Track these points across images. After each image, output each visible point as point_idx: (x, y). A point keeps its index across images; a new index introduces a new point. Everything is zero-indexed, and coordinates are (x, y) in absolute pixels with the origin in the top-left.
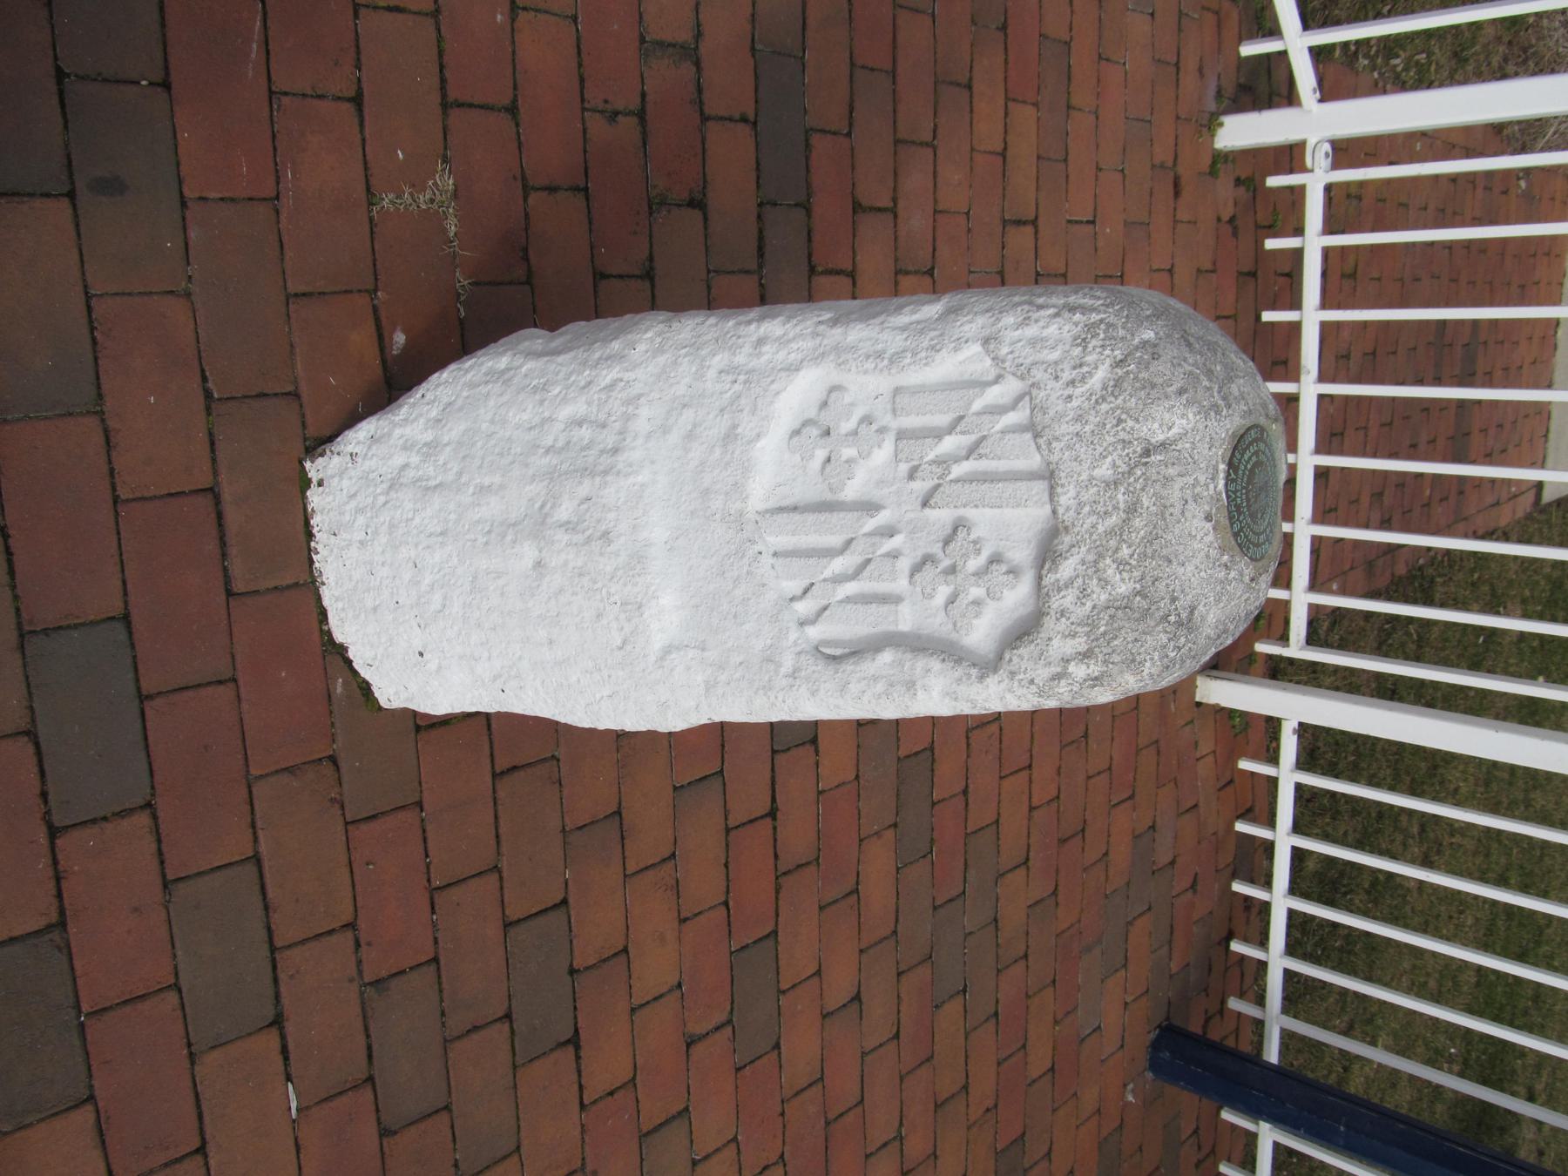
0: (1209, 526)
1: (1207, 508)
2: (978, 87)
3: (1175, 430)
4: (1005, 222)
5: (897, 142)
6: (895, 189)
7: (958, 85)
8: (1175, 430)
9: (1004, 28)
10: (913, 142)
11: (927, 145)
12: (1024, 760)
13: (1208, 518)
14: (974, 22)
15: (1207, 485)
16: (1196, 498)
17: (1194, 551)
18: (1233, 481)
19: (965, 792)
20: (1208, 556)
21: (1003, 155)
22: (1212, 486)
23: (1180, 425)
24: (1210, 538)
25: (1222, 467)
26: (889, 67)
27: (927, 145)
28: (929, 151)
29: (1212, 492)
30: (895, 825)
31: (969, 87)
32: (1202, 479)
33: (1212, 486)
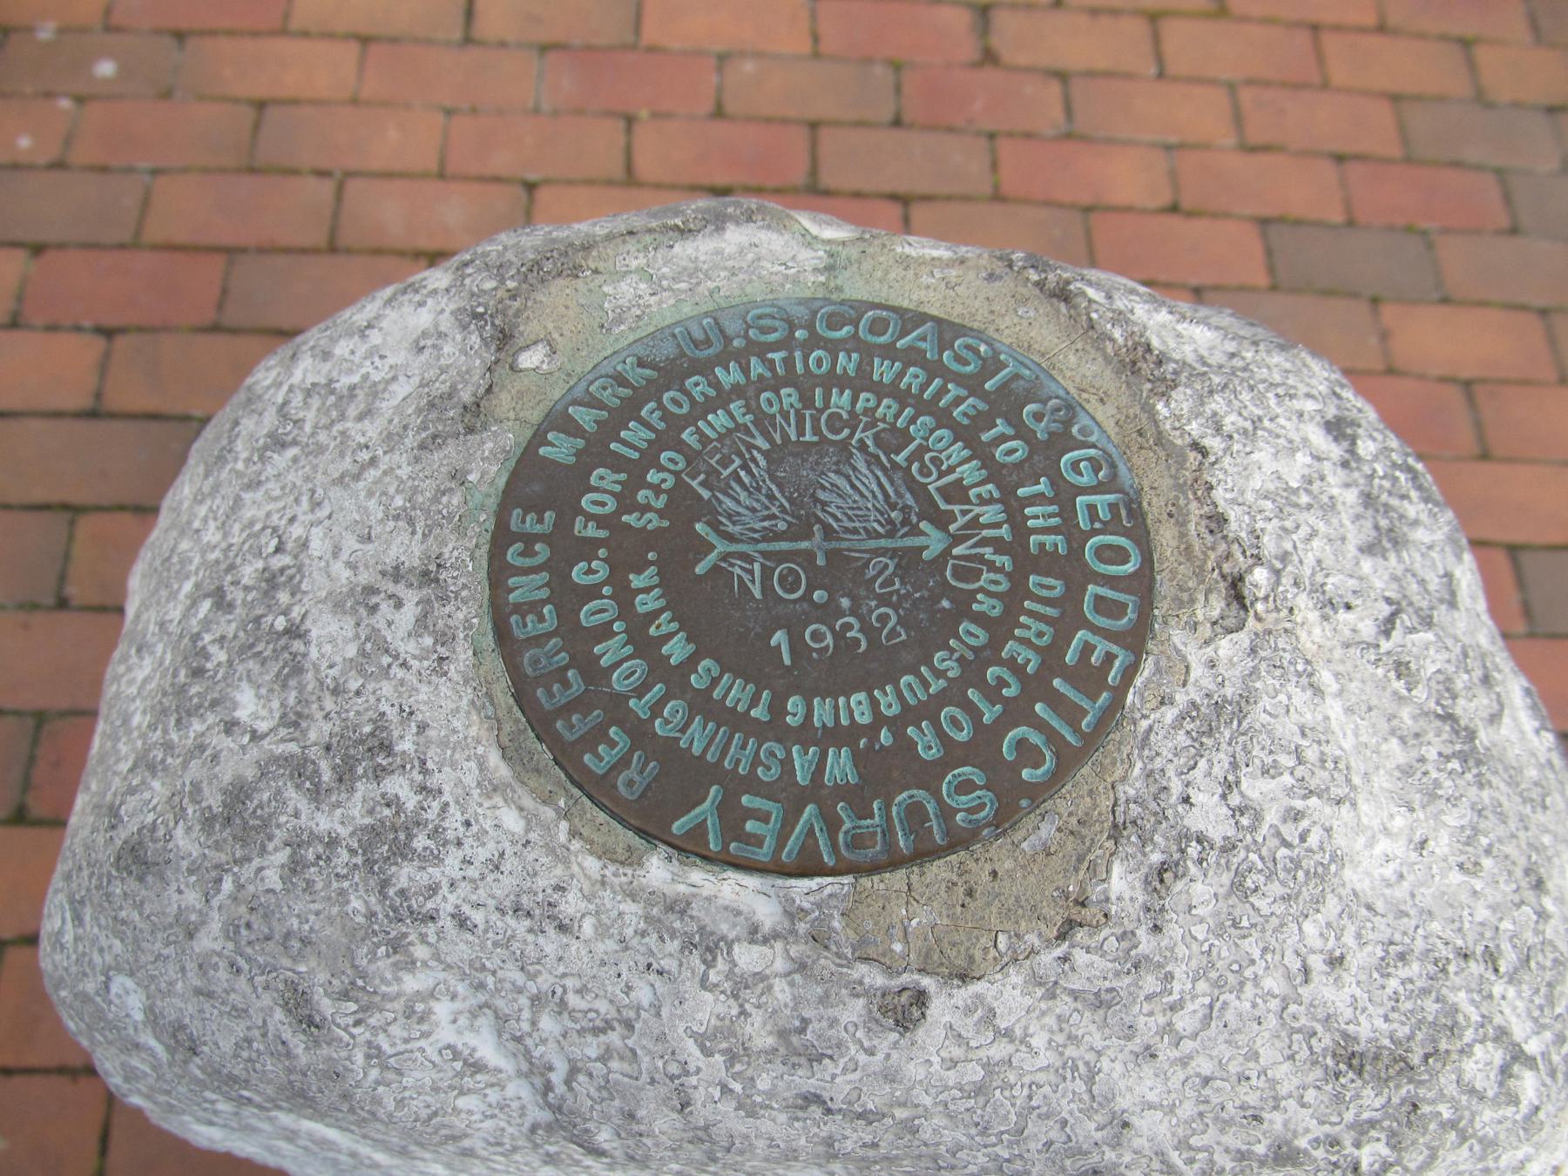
0: (945, 1006)
1: (853, 1011)
2: (260, 91)
3: (487, 1048)
4: (468, 40)
5: (333, 249)
6: (401, 254)
7: (257, 126)
8: (487, 1048)
9: (180, 36)
10: (336, 215)
11: (340, 189)
12: (1302, 38)
13: (905, 1012)
14: (166, 95)
15: (740, 985)
16: (799, 1046)
17: (1066, 1069)
18: (732, 818)
19: (1340, 159)
20: (1101, 1002)
21: (365, 40)
22: (748, 957)
23: (447, 1024)
24: (1008, 993)
25: (658, 870)
26: (220, 261)
27: (340, 189)
28: (353, 186)
29: (773, 959)
30: (1375, 301)
31: (261, 105)
32: (708, 1008)
33: (748, 957)
